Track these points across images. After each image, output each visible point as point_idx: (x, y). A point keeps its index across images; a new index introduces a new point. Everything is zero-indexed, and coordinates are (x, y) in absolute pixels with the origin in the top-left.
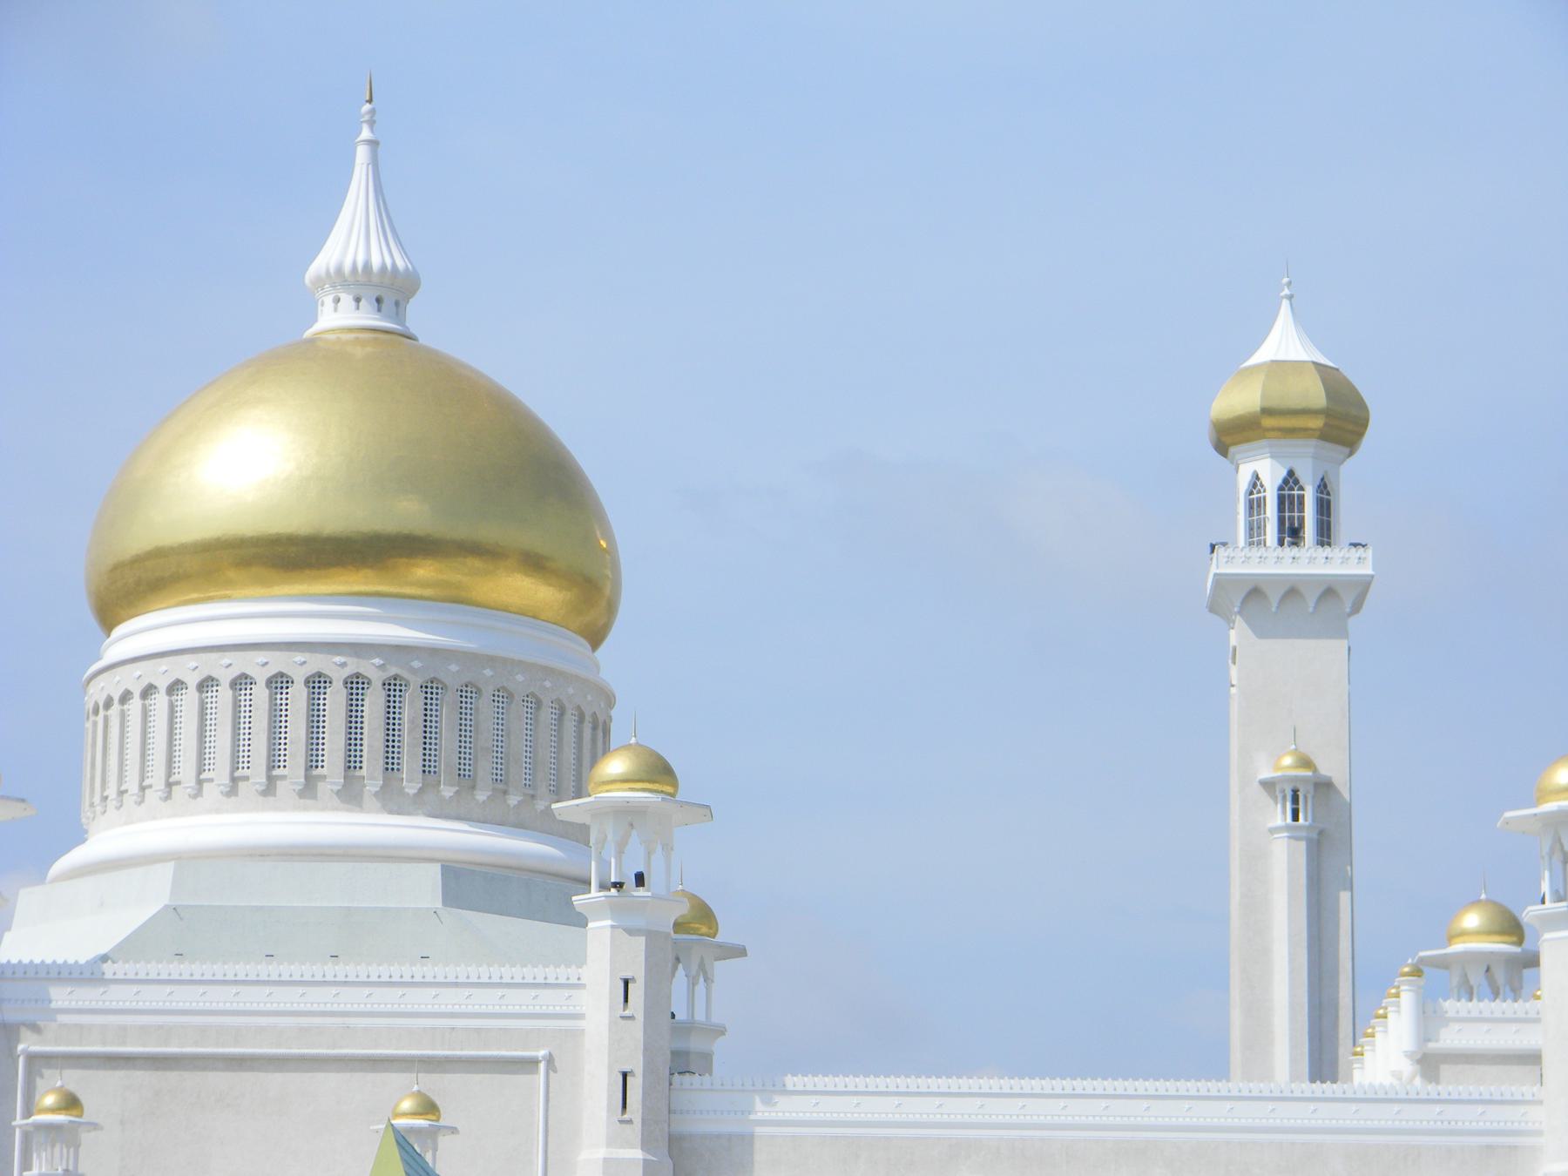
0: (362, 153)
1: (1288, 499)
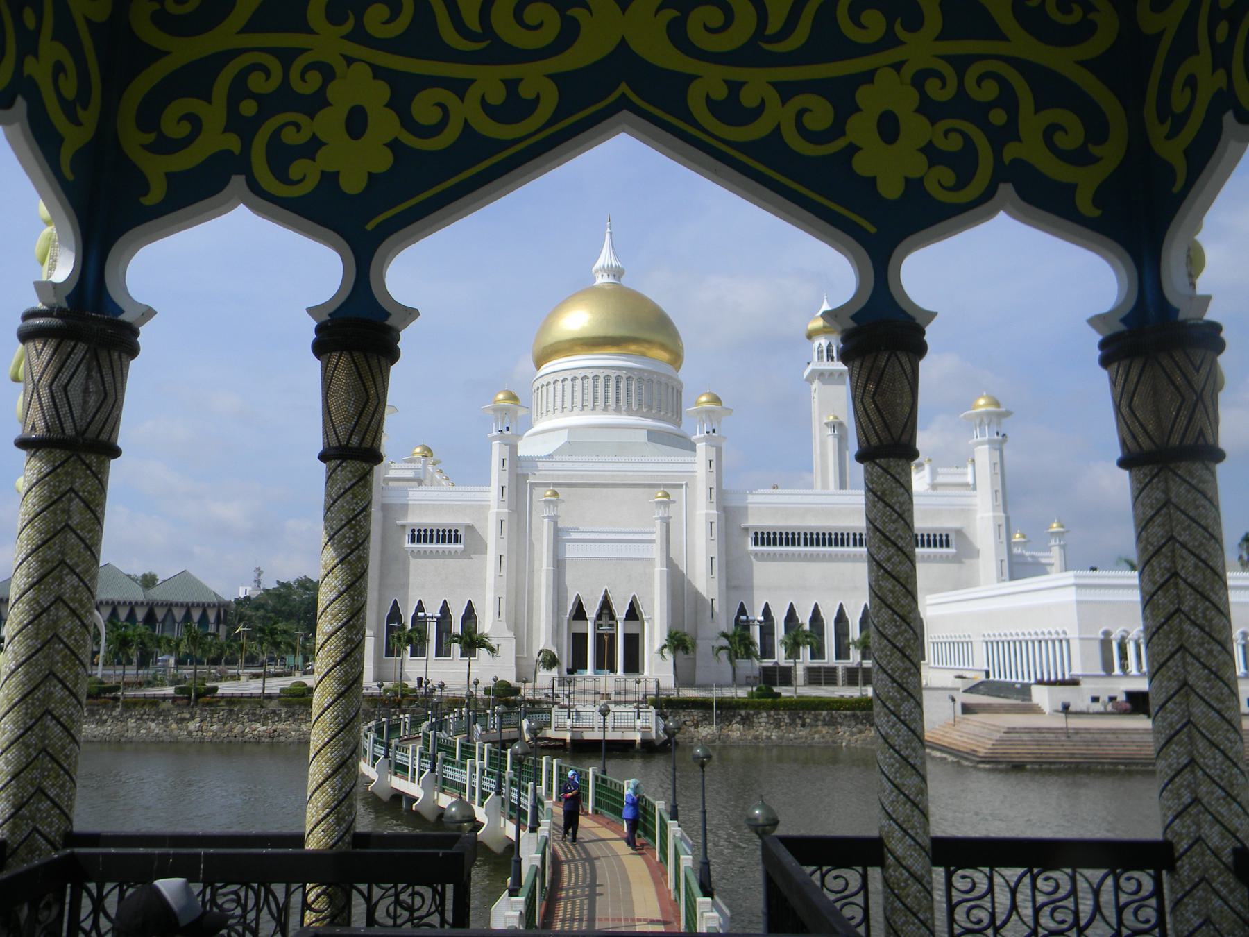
0: (608, 236)
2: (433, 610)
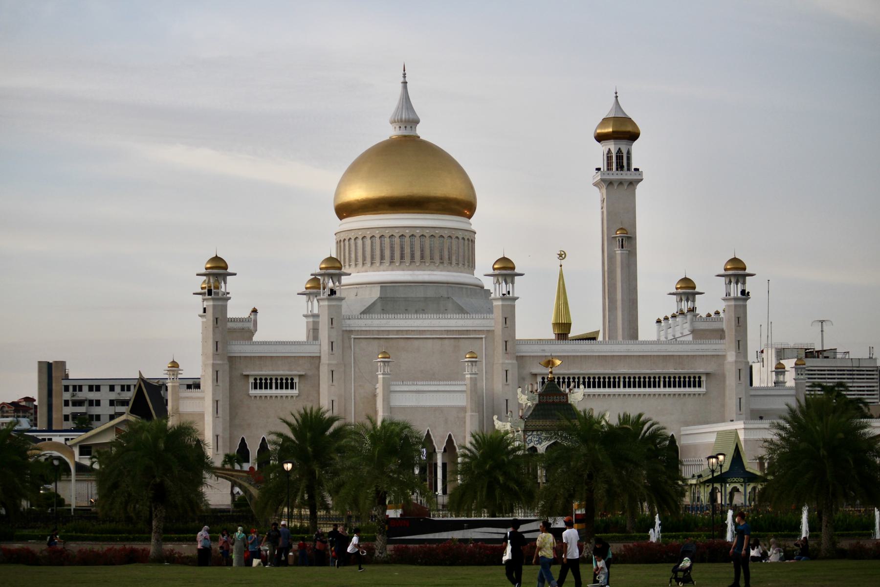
1: (619, 157)
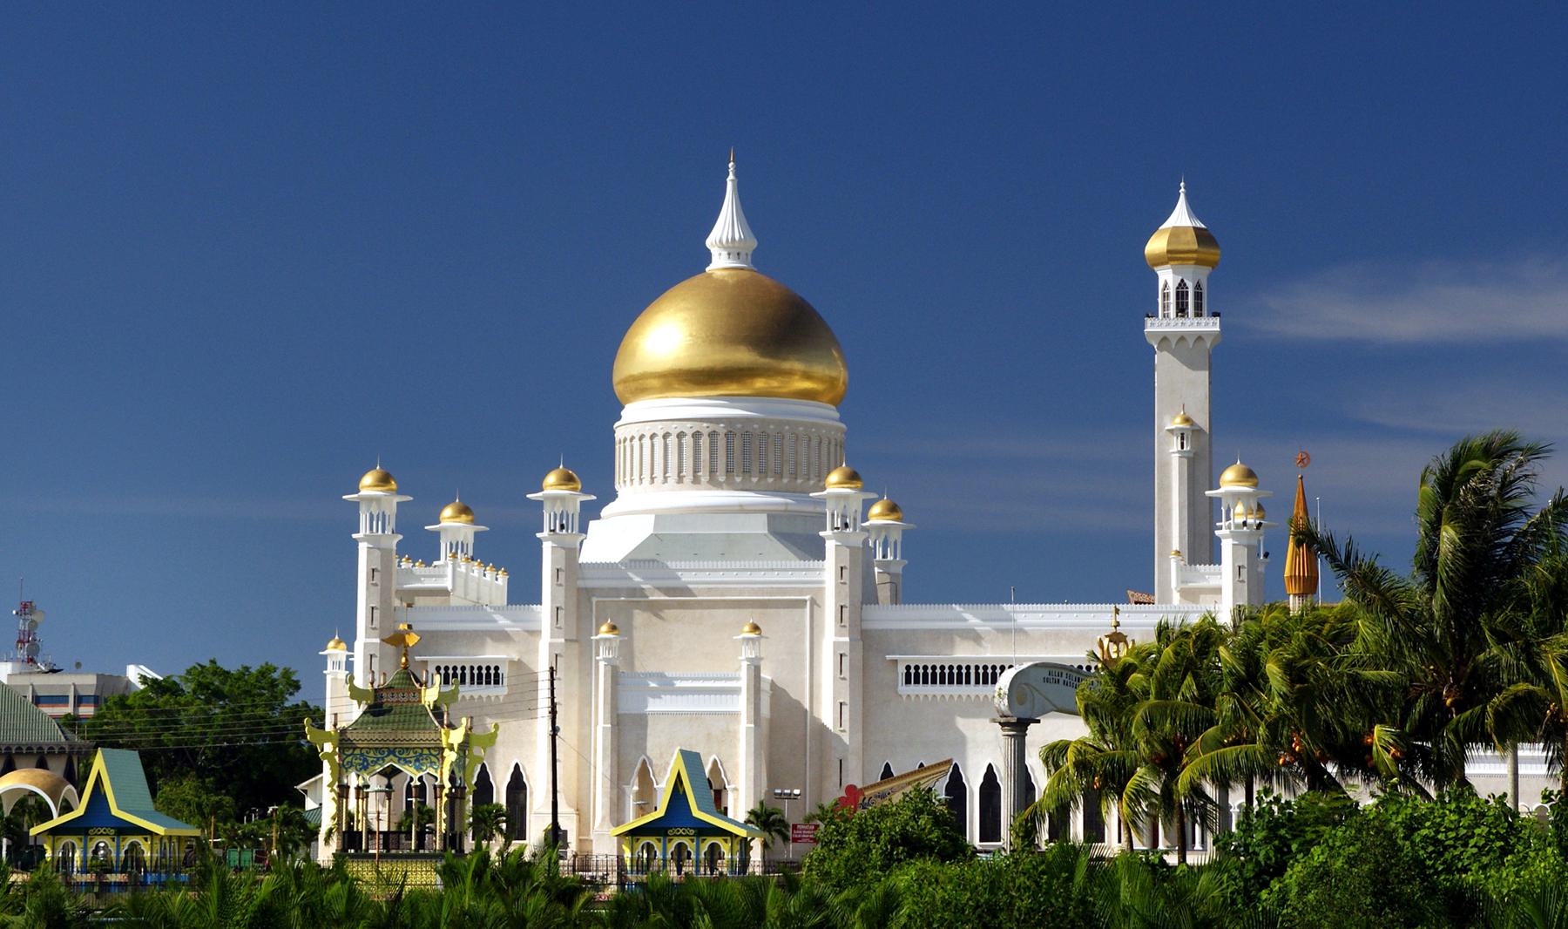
2: (974, 783)
